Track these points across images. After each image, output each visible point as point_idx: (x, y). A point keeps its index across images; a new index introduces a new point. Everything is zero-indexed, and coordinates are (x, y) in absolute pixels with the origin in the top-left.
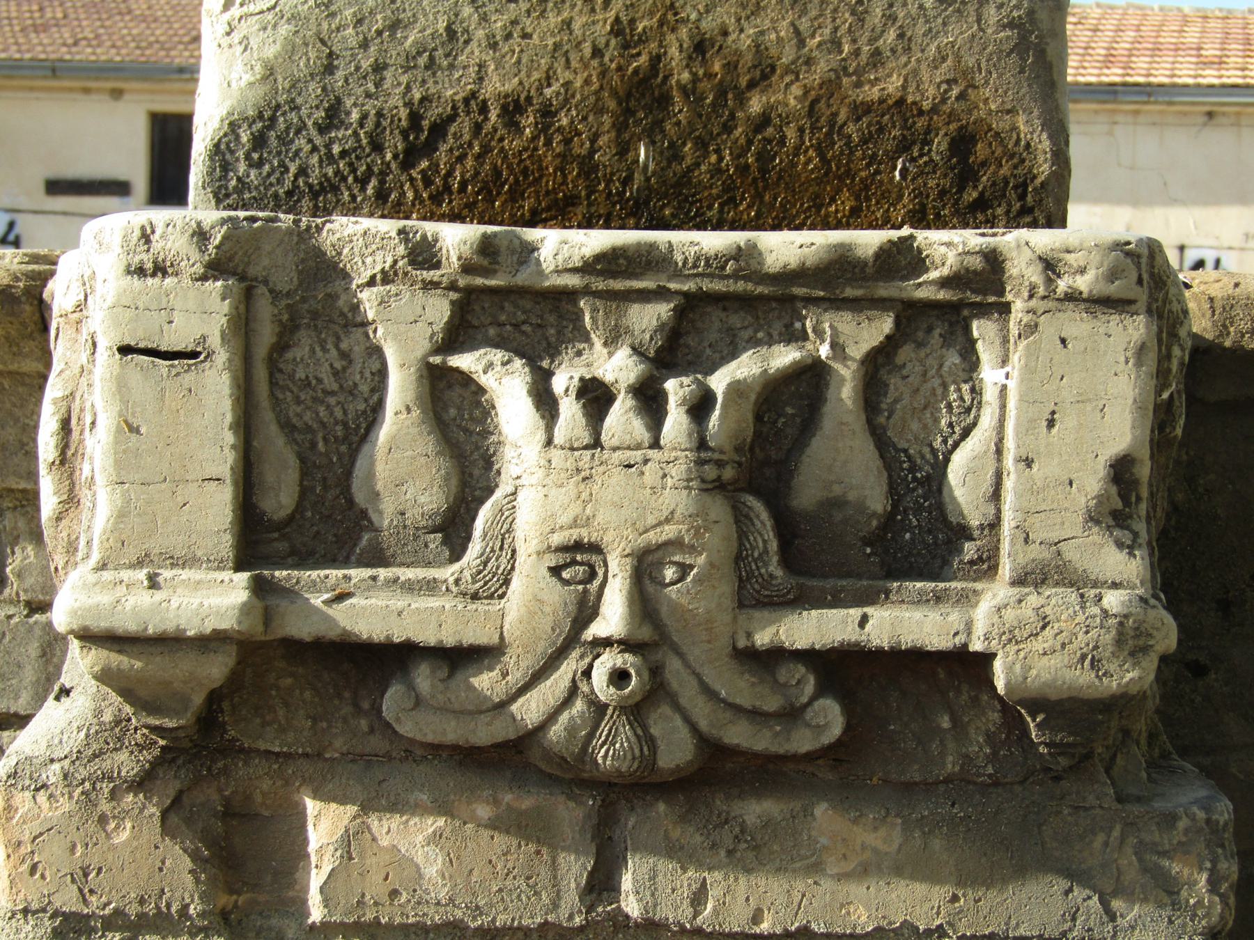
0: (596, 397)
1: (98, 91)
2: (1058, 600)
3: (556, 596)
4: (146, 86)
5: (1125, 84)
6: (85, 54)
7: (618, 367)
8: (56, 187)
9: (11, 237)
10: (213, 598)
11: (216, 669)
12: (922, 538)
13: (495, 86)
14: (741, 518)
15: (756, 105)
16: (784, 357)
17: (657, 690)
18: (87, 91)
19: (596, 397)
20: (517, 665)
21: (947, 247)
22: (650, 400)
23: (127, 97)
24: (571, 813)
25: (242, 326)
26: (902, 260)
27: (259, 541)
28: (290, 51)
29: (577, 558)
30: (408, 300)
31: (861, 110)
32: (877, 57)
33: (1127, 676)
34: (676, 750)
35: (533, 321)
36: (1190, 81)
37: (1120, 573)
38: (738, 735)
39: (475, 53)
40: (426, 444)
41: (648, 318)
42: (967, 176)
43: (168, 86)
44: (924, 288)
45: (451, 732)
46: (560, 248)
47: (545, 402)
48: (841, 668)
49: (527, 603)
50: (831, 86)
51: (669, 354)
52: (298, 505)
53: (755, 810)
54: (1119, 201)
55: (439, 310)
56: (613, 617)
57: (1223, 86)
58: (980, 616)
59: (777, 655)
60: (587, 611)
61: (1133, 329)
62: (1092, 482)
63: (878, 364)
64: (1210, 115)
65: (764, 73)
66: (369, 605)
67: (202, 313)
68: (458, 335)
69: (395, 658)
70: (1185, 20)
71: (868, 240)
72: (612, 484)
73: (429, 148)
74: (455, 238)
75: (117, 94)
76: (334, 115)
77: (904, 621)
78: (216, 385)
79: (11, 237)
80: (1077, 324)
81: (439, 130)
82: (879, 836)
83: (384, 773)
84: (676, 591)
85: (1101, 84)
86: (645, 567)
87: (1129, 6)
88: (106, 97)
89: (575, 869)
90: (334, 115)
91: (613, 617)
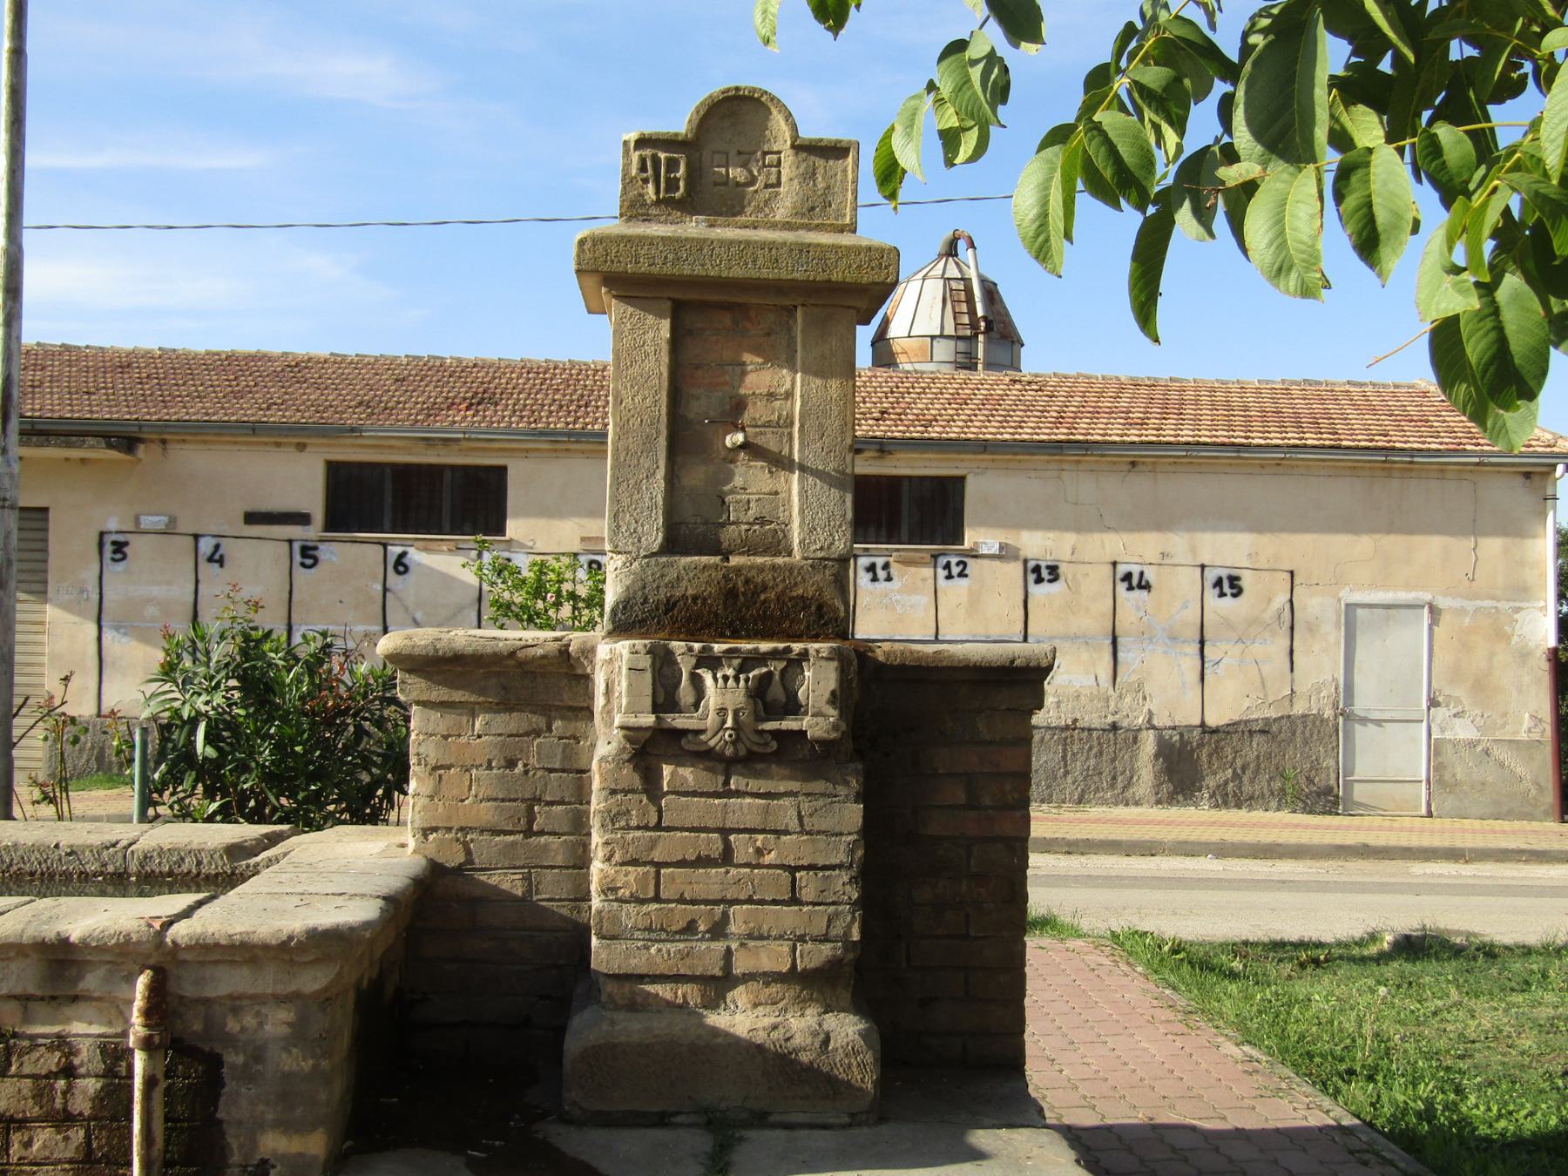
0: (726, 678)
1: (286, 444)
2: (820, 719)
3: (718, 719)
4: (325, 441)
5: (1069, 442)
6: (275, 416)
7: (730, 672)
8: (252, 518)
9: (217, 557)
10: (648, 720)
11: (648, 735)
12: (793, 707)
13: (690, 592)
14: (755, 703)
15: (762, 597)
16: (764, 670)
17: (738, 739)
18: (278, 445)
19: (726, 678)
20: (709, 734)
21: (797, 647)
22: (737, 679)
23: (309, 449)
24: (720, 767)
25: (653, 665)
26: (788, 650)
27: (656, 709)
28: (633, 582)
29: (722, 711)
30: (686, 658)
31: (791, 599)
32: (796, 584)
33: (834, 735)
34: (742, 752)
35: (712, 662)
36: (1117, 439)
37: (833, 713)
38: (755, 749)
39: (684, 583)
40: (690, 688)
41: (736, 662)
42: (821, 616)
43: (341, 441)
44: (792, 656)
45: (696, 748)
46: (718, 647)
47: (715, 679)
48: (777, 734)
49: (712, 720)
50: (783, 592)
51: (741, 669)
52: (664, 700)
53: (759, 766)
54: (1066, 529)
55: (694, 661)
56: (729, 723)
57: (1142, 443)
58: (805, 723)
59: (763, 731)
60: (724, 722)
61: (835, 664)
62: (827, 695)
63: (783, 672)
64: (1133, 464)
65: (765, 588)
66: (679, 721)
67: (645, 662)
68: (697, 666)
69: (684, 732)
70: (1122, 388)
71: (781, 646)
72: (729, 696)
73: (672, 609)
74: (697, 646)
75: (301, 447)
76: (646, 600)
77: (789, 724)
78: (648, 676)
79: (217, 557)
80: (823, 663)
81: (675, 604)
82: (785, 772)
83: (681, 758)
84: (742, 717)
85: (1050, 441)
86: (736, 713)
87: (1079, 375)
88: (293, 449)
89: (721, 779)
90: (646, 600)
91: (729, 723)
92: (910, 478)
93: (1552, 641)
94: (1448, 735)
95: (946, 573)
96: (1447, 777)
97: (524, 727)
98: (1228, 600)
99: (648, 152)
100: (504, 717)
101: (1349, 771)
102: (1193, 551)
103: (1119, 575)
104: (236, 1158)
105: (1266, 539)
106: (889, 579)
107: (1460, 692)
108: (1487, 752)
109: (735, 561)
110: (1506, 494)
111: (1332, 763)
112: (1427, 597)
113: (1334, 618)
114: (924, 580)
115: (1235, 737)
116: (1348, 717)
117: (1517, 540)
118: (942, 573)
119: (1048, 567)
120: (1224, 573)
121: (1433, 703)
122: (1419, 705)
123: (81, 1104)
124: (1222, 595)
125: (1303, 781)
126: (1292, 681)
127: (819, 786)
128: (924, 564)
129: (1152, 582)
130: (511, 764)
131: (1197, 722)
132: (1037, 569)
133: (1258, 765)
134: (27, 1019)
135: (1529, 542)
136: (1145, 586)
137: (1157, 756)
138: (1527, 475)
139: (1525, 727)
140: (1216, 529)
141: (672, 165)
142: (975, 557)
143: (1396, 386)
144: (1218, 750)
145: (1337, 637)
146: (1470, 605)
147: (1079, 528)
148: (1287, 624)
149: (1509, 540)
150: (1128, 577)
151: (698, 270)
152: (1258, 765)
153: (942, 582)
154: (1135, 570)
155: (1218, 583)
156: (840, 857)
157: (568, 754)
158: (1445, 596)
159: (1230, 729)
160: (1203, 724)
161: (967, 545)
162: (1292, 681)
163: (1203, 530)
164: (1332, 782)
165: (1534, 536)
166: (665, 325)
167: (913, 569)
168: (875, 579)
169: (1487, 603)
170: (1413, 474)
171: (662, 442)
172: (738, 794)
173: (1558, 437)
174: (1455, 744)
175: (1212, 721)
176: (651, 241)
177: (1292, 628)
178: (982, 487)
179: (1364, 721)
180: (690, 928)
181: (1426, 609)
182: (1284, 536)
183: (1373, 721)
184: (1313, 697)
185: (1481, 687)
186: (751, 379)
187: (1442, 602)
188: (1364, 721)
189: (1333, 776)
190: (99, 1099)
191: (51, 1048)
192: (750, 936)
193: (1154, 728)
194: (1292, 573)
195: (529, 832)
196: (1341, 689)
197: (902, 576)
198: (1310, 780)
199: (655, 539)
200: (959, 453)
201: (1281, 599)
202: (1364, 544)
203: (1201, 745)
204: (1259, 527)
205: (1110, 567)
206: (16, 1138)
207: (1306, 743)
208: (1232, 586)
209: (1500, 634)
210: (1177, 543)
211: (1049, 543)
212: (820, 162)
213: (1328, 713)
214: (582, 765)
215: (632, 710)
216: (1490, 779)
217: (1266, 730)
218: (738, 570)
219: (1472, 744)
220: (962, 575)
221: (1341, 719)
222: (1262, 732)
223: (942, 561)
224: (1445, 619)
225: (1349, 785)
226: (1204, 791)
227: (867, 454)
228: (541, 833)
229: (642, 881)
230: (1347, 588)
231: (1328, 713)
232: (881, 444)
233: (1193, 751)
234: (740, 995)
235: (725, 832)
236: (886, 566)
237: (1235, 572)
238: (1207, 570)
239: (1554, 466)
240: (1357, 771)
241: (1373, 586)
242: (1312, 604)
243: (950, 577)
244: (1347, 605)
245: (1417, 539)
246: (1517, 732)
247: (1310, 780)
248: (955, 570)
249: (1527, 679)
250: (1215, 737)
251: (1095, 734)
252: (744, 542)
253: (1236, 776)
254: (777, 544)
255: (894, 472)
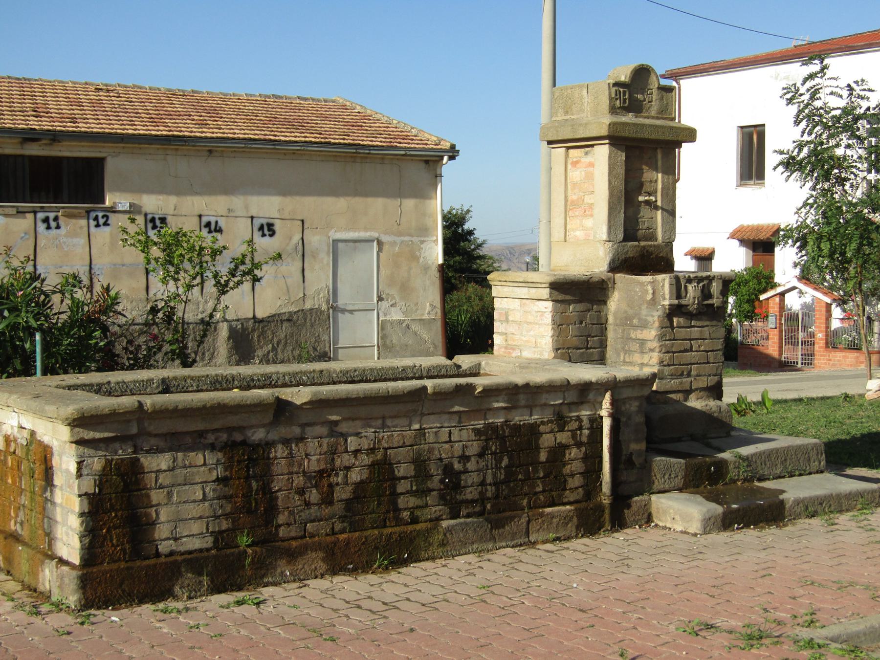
64: (210, 151)
77: (709, 302)
92: (68, 158)
93: (441, 261)
94: (388, 318)
95: (95, 223)
96: (388, 343)
97: (586, 308)
98: (267, 238)
99: (616, 88)
100: (578, 305)
101: (336, 342)
102: (247, 208)
103: (203, 224)
104: (624, 453)
105: (288, 200)
106: (58, 227)
107: (394, 292)
108: (408, 327)
109: (643, 243)
110: (416, 173)
111: (327, 338)
112: (376, 235)
113: (326, 248)
114: (81, 228)
115: (273, 324)
116: (335, 309)
117: (422, 200)
118: (93, 223)
119: (160, 219)
120: (264, 221)
121: (380, 299)
122: (373, 300)
123: (584, 439)
124: (264, 235)
125: (311, 349)
126: (304, 288)
127: (714, 323)
128: (81, 217)
129: (223, 228)
130: (581, 323)
131: (251, 316)
132: (153, 220)
133: (286, 341)
134: (570, 411)
135: (428, 202)
136: (219, 230)
137: (229, 338)
138: (427, 162)
139: (427, 311)
140: (260, 194)
141: (624, 93)
142: (115, 212)
143: (325, 101)
144: (263, 334)
145: (328, 260)
146: (398, 239)
147: (178, 193)
148: (300, 253)
149: (418, 200)
150: (208, 225)
151: (642, 136)
152: (286, 341)
153: (93, 229)
154: (213, 220)
155: (261, 228)
156: (720, 347)
157: (599, 317)
158: (385, 234)
159: (270, 319)
160: (254, 317)
161: (108, 203)
162: (304, 288)
163: (252, 194)
164: (327, 349)
165: (431, 198)
166: (624, 154)
167: (74, 221)
168: (49, 228)
169: (407, 238)
170: (368, 160)
171: (623, 199)
172: (694, 327)
173: (440, 140)
174: (392, 323)
175: (260, 315)
176: (643, 125)
177: (303, 256)
178: (112, 167)
179: (343, 311)
180: (682, 374)
181: (375, 243)
182: (298, 198)
183: (347, 311)
184: (316, 300)
185: (405, 288)
186: (645, 175)
187: (384, 238)
188: (343, 311)
189: (327, 345)
190: (589, 436)
191: (576, 421)
192: (698, 376)
193: (226, 320)
194: (303, 221)
195: (587, 348)
196: (331, 292)
197: (67, 226)
198: (315, 349)
199: (621, 236)
200: (104, 142)
201: (297, 238)
202: (341, 203)
203: (254, 330)
204: (284, 192)
205: (198, 218)
206: (567, 452)
207: (312, 326)
208: (269, 230)
209: (414, 257)
210: (237, 202)
211: (160, 203)
212: (664, 94)
213: (324, 307)
214: (603, 321)
215: (670, 299)
216: (410, 343)
217: (290, 319)
218: (644, 247)
219: (401, 322)
220: (106, 224)
221: (331, 310)
222: (288, 320)
223: (93, 215)
224: (386, 248)
225: (336, 350)
226: (256, 359)
227: (44, 142)
228: (591, 348)
229: (670, 359)
230: (333, 230)
231: (324, 307)
232: (54, 135)
233: (249, 334)
234: (693, 396)
235: (690, 340)
236: (56, 219)
237: (271, 221)
238: (255, 220)
239: (442, 158)
240: (340, 342)
241: (348, 229)
242: (314, 240)
243: (98, 226)
244: (333, 241)
245: (370, 200)
246: (423, 315)
247: (315, 349)
248: (101, 221)
249: (428, 283)
250: (262, 325)
251: (191, 327)
252: (644, 236)
253: (274, 349)
254: (652, 237)
255: (59, 154)
